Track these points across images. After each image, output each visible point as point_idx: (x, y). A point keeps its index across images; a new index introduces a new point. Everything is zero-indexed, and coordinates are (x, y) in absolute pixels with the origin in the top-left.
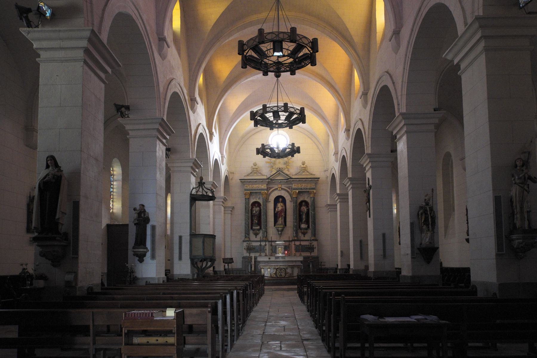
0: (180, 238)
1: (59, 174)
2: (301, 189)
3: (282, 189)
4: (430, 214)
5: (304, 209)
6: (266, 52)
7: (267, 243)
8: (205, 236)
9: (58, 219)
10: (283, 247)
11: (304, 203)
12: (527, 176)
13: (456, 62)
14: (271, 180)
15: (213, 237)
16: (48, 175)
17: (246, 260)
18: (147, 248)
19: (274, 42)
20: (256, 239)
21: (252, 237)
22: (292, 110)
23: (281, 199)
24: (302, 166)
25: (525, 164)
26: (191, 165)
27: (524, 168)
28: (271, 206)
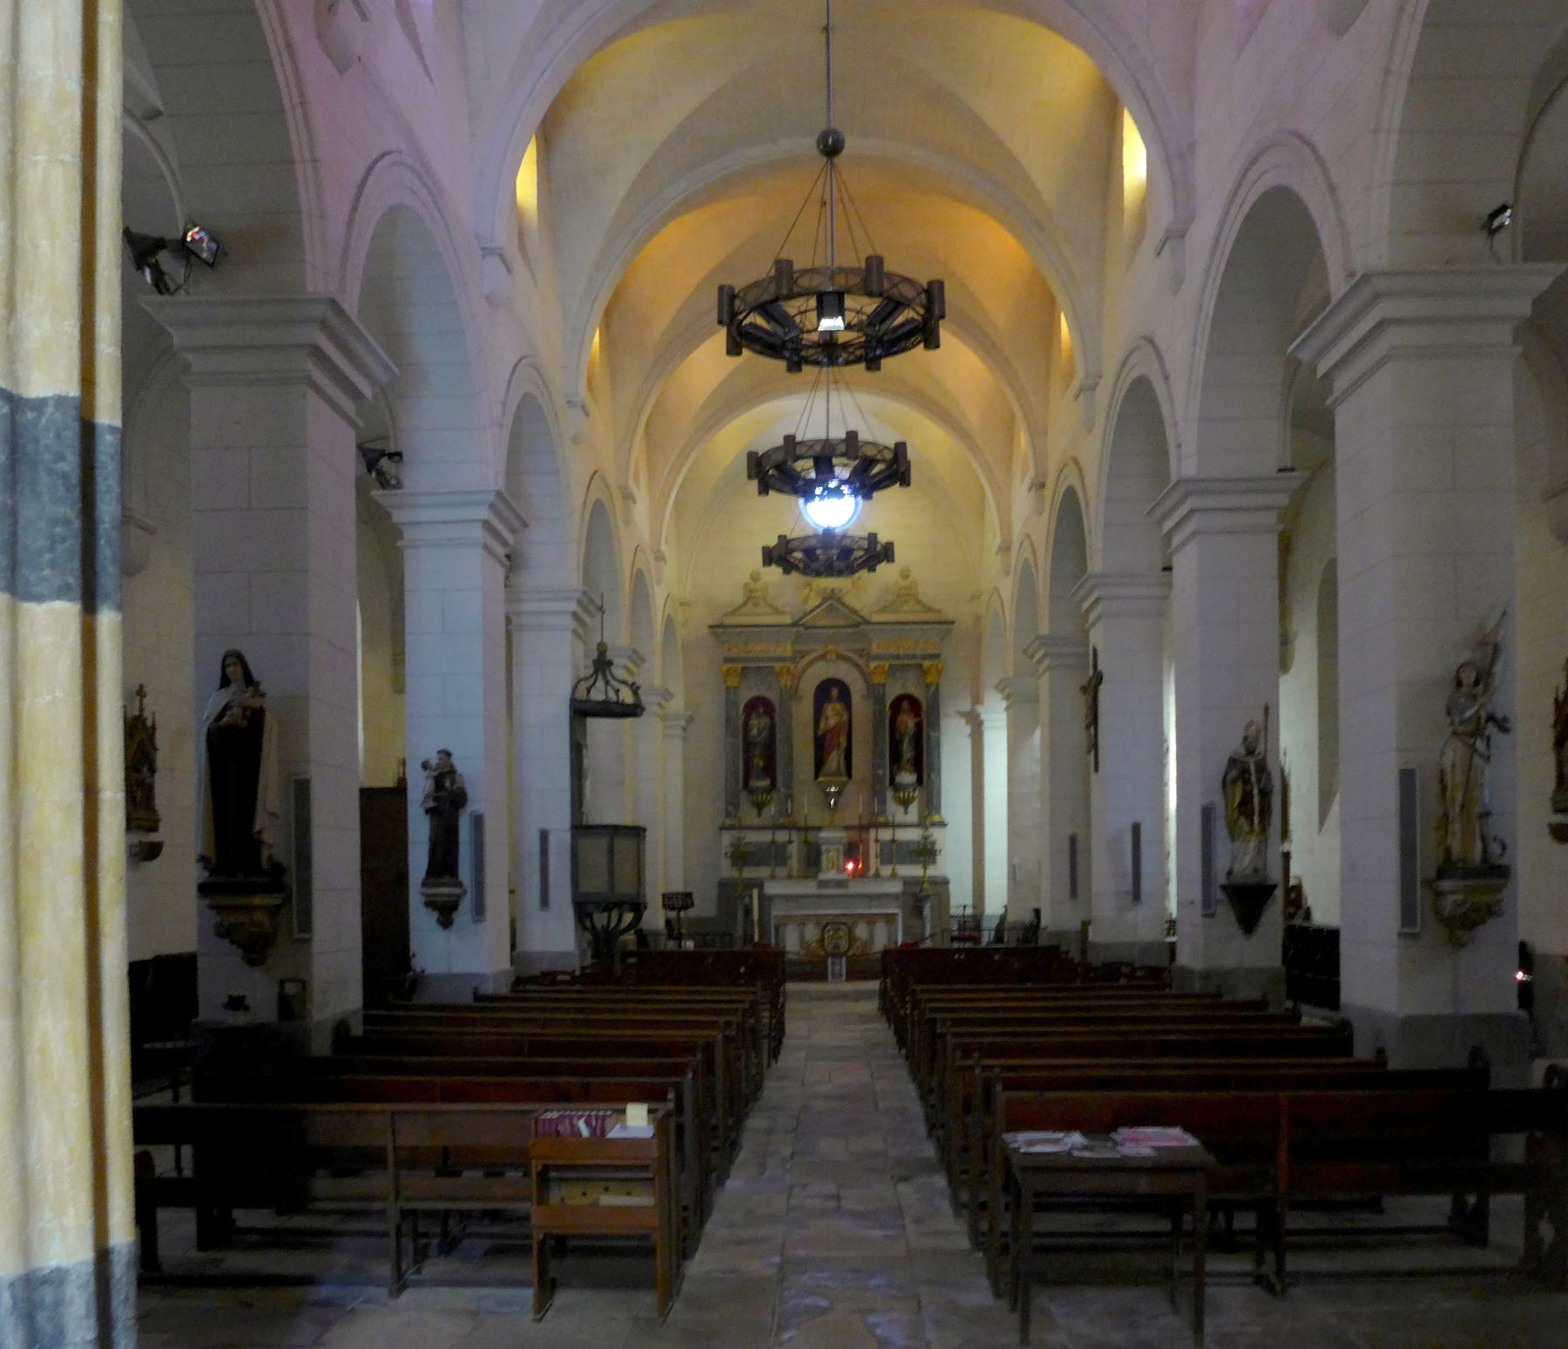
0: (544, 836)
1: (257, 703)
2: (898, 657)
3: (840, 657)
4: (1259, 781)
5: (908, 722)
6: (798, 319)
7: (794, 835)
8: (615, 830)
9: (260, 832)
10: (841, 847)
11: (905, 705)
12: (1483, 715)
13: (1323, 367)
14: (807, 628)
15: (637, 832)
16: (227, 707)
17: (731, 894)
18: (459, 884)
19: (821, 296)
20: (757, 821)
21: (748, 814)
22: (870, 452)
23: (835, 692)
24: (903, 583)
25: (1483, 678)
26: (573, 606)
27: (1480, 689)
28: (804, 710)
